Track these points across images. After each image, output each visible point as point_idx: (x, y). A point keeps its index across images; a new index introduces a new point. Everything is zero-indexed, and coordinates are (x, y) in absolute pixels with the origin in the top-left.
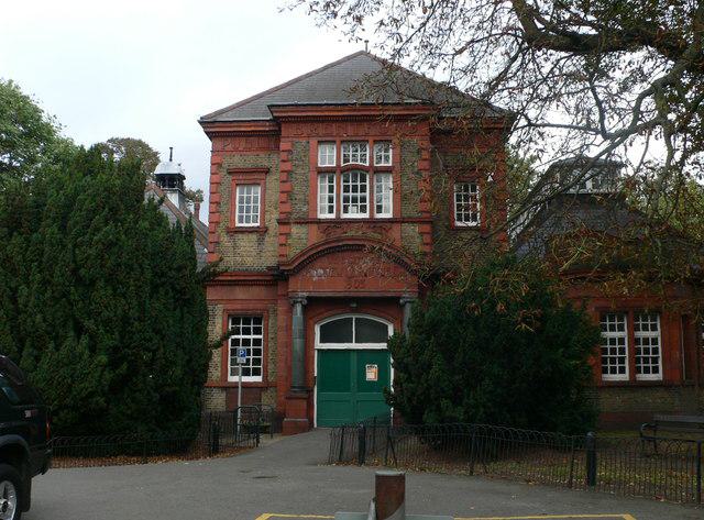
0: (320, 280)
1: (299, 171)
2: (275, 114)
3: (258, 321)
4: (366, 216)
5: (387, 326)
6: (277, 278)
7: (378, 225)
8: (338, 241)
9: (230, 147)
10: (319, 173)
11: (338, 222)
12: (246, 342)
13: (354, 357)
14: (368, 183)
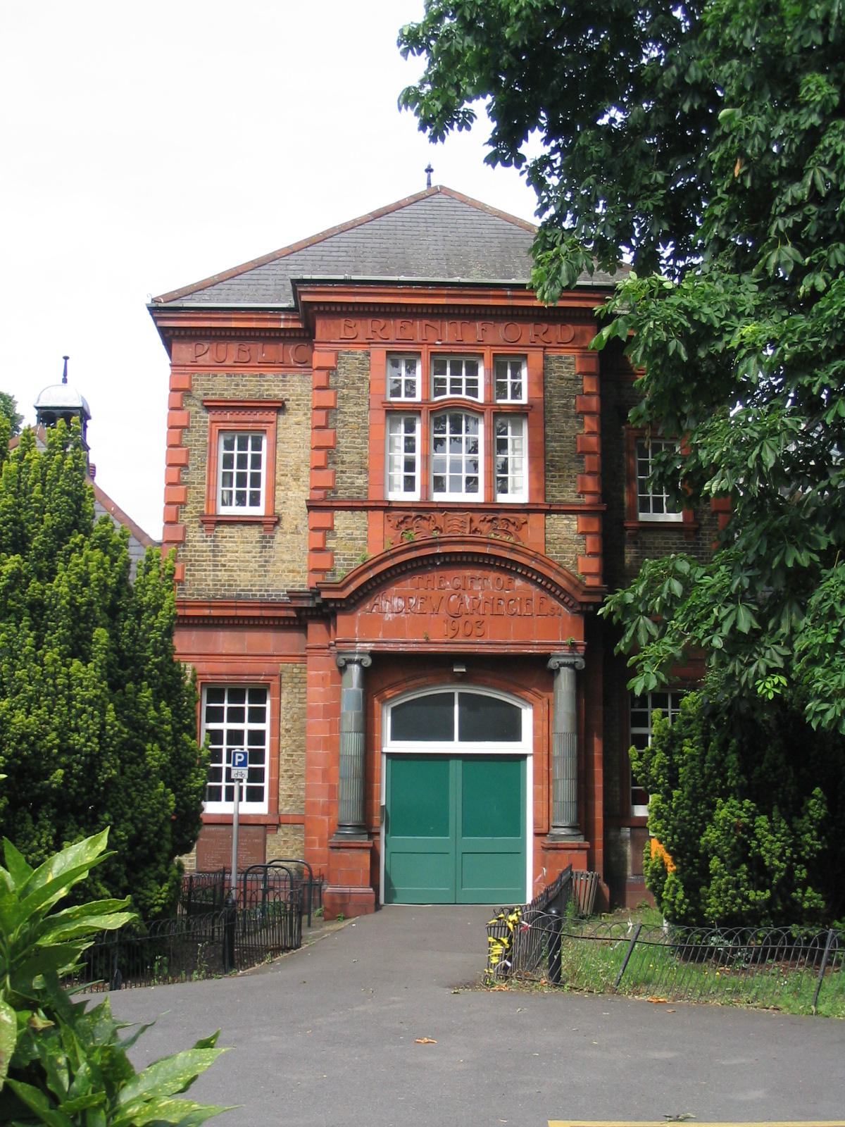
0: (397, 620)
1: (350, 408)
2: (305, 298)
3: (259, 695)
4: (478, 497)
6: (313, 611)
7: (501, 516)
9: (206, 359)
11: (425, 510)
12: (235, 737)
14: (264, 453)
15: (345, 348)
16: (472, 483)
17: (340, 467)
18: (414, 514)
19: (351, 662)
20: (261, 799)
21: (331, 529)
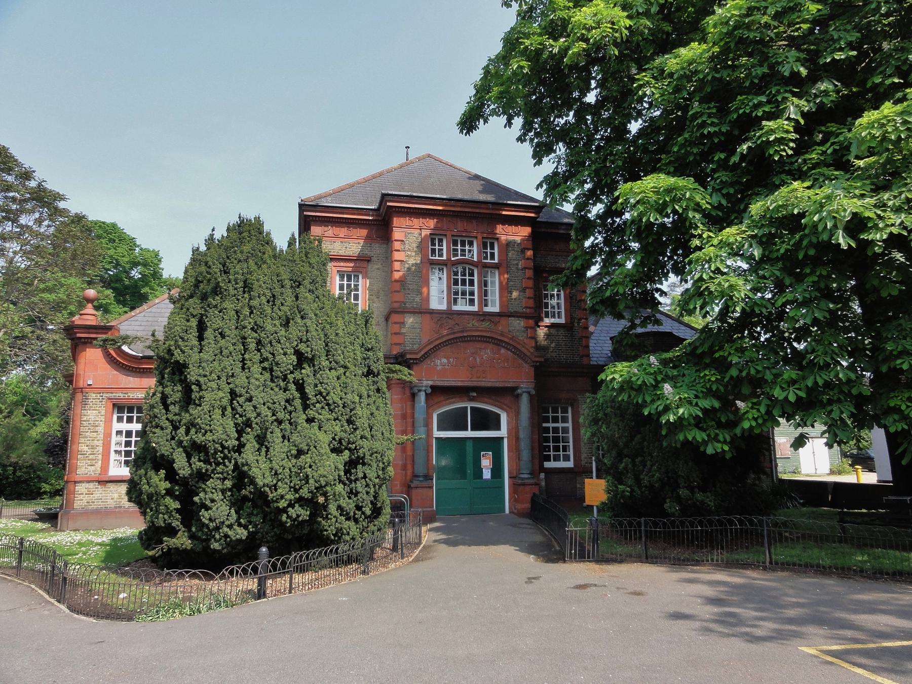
4: (475, 308)
5: (499, 415)
7: (487, 318)
8: (463, 332)
10: (431, 264)
13: (469, 446)
15: (409, 231)
16: (472, 302)
17: (407, 291)
18: (444, 316)
19: (420, 391)
20: (569, 460)
21: (403, 323)
